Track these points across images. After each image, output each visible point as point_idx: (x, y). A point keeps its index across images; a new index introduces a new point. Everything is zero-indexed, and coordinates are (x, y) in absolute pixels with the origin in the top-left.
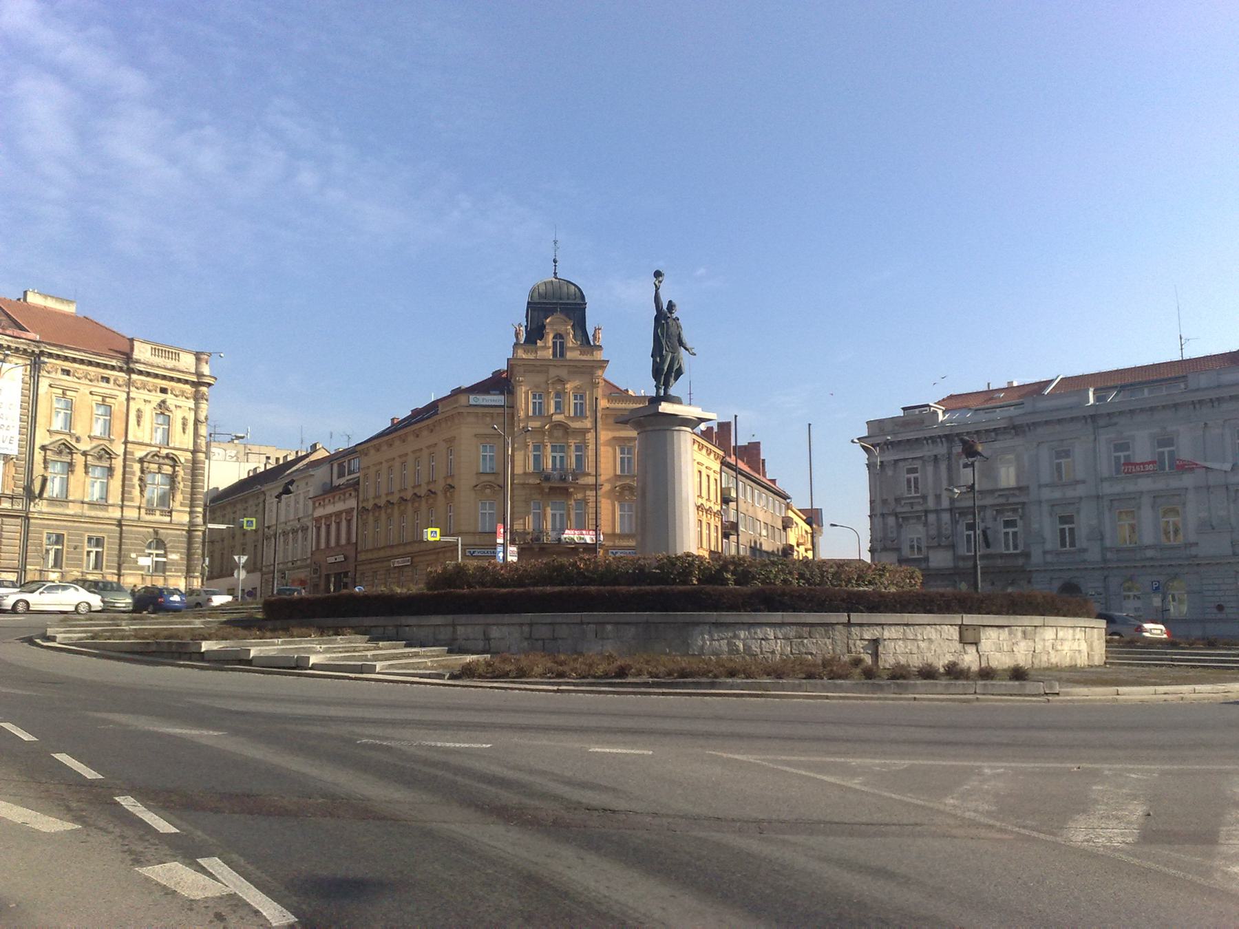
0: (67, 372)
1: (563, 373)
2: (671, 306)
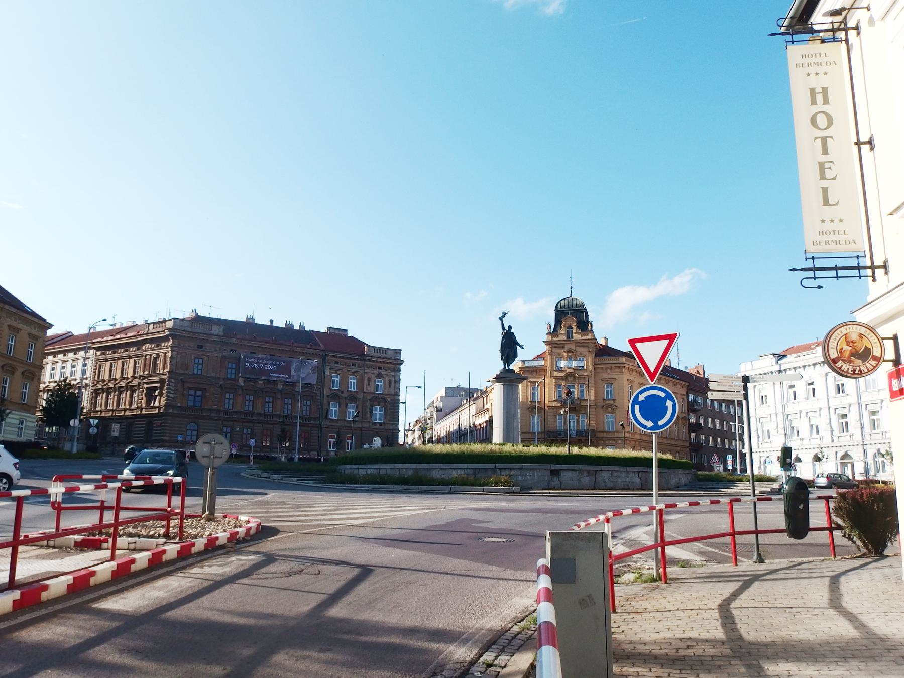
0: (337, 363)
1: (573, 347)
2: (510, 327)
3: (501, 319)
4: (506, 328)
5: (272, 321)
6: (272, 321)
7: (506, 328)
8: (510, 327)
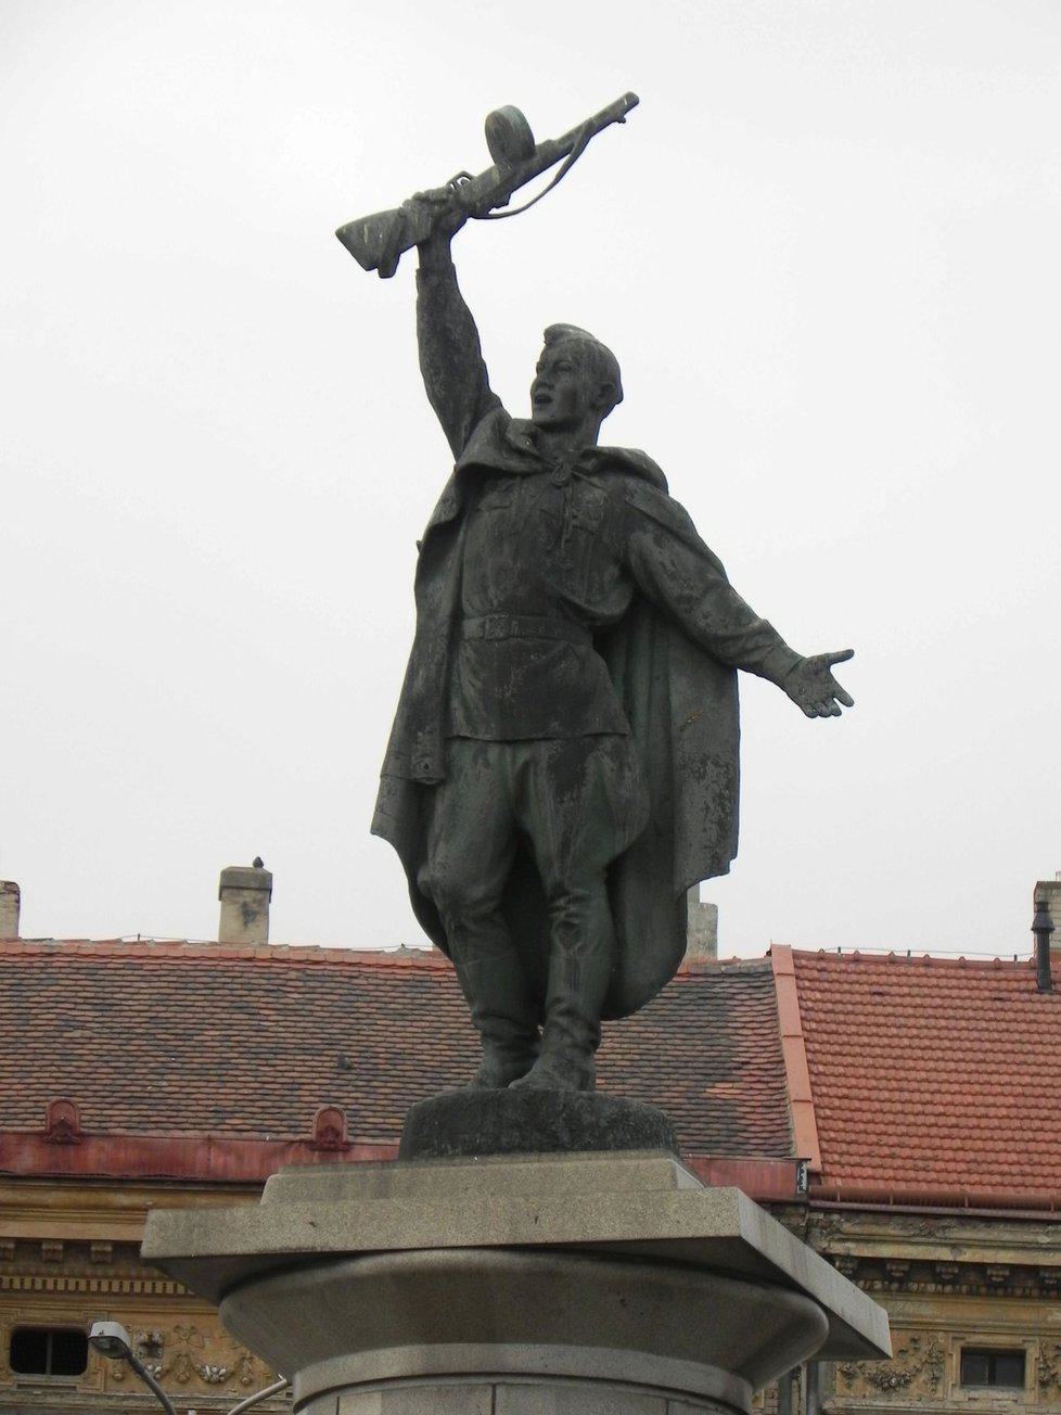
3: (414, 237)
4: (513, 385)
5: (247, 889)
6: (247, 889)
7: (513, 385)
8: (580, 376)
